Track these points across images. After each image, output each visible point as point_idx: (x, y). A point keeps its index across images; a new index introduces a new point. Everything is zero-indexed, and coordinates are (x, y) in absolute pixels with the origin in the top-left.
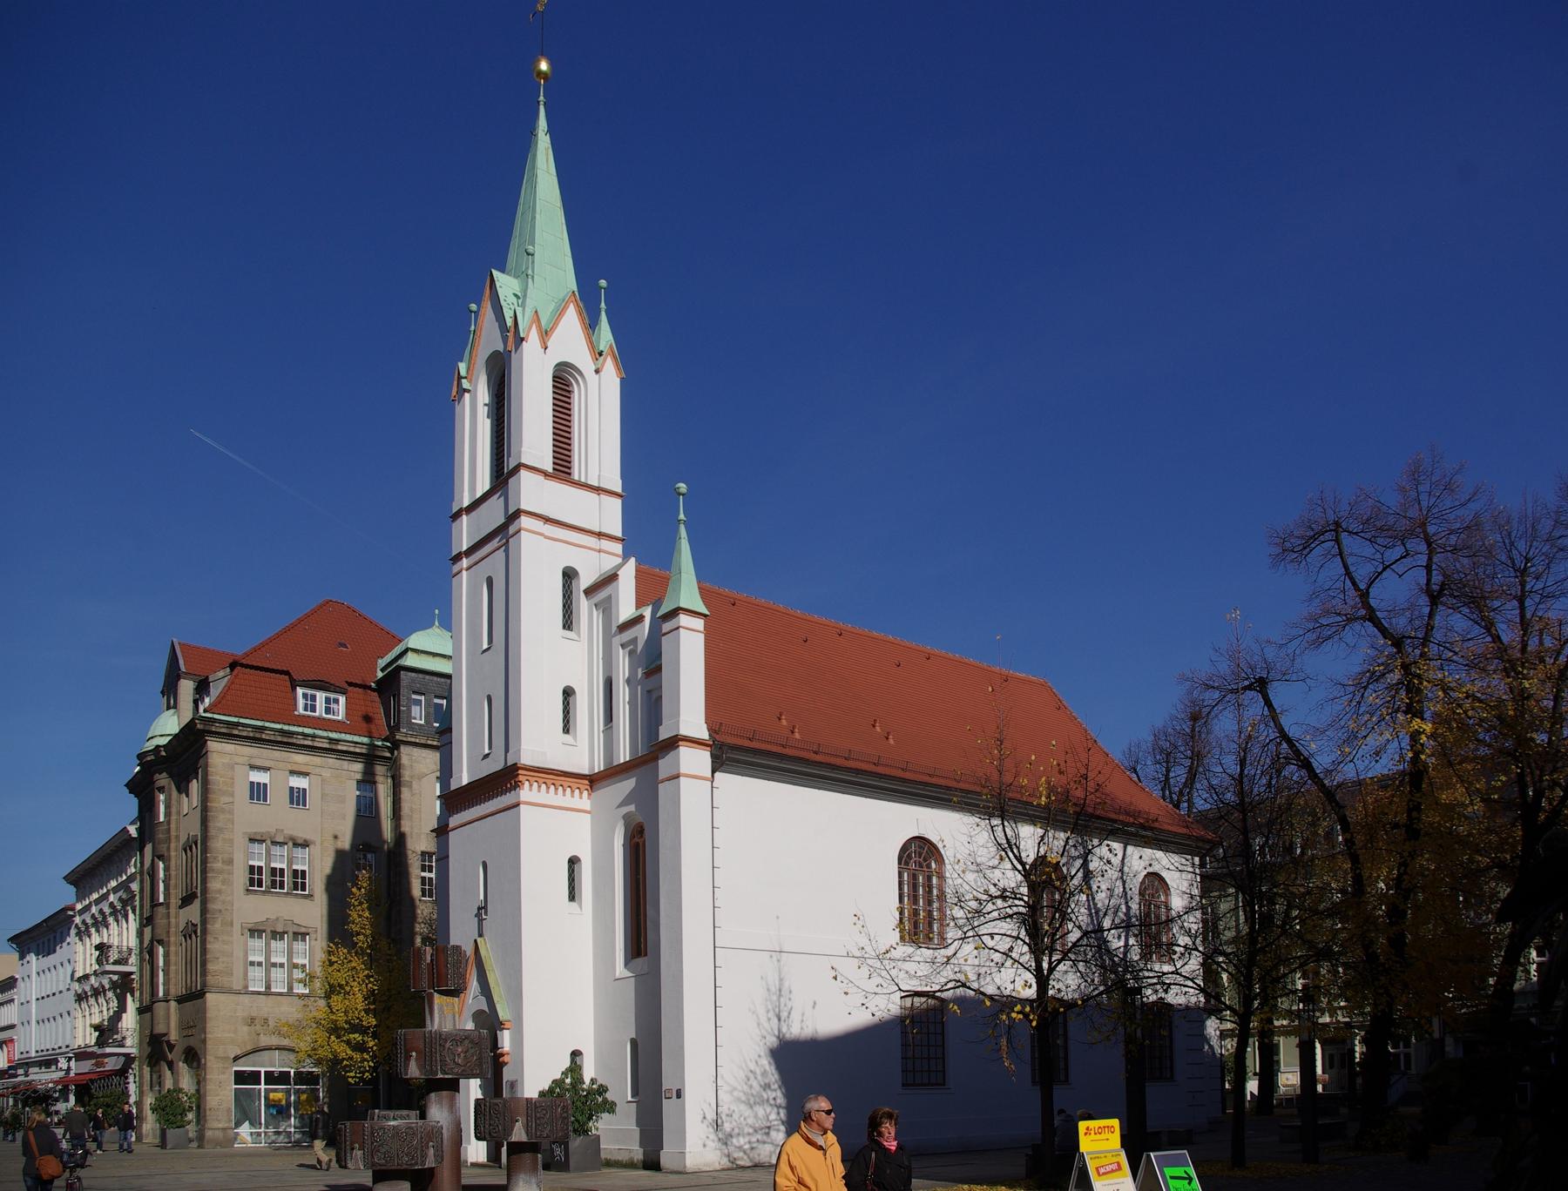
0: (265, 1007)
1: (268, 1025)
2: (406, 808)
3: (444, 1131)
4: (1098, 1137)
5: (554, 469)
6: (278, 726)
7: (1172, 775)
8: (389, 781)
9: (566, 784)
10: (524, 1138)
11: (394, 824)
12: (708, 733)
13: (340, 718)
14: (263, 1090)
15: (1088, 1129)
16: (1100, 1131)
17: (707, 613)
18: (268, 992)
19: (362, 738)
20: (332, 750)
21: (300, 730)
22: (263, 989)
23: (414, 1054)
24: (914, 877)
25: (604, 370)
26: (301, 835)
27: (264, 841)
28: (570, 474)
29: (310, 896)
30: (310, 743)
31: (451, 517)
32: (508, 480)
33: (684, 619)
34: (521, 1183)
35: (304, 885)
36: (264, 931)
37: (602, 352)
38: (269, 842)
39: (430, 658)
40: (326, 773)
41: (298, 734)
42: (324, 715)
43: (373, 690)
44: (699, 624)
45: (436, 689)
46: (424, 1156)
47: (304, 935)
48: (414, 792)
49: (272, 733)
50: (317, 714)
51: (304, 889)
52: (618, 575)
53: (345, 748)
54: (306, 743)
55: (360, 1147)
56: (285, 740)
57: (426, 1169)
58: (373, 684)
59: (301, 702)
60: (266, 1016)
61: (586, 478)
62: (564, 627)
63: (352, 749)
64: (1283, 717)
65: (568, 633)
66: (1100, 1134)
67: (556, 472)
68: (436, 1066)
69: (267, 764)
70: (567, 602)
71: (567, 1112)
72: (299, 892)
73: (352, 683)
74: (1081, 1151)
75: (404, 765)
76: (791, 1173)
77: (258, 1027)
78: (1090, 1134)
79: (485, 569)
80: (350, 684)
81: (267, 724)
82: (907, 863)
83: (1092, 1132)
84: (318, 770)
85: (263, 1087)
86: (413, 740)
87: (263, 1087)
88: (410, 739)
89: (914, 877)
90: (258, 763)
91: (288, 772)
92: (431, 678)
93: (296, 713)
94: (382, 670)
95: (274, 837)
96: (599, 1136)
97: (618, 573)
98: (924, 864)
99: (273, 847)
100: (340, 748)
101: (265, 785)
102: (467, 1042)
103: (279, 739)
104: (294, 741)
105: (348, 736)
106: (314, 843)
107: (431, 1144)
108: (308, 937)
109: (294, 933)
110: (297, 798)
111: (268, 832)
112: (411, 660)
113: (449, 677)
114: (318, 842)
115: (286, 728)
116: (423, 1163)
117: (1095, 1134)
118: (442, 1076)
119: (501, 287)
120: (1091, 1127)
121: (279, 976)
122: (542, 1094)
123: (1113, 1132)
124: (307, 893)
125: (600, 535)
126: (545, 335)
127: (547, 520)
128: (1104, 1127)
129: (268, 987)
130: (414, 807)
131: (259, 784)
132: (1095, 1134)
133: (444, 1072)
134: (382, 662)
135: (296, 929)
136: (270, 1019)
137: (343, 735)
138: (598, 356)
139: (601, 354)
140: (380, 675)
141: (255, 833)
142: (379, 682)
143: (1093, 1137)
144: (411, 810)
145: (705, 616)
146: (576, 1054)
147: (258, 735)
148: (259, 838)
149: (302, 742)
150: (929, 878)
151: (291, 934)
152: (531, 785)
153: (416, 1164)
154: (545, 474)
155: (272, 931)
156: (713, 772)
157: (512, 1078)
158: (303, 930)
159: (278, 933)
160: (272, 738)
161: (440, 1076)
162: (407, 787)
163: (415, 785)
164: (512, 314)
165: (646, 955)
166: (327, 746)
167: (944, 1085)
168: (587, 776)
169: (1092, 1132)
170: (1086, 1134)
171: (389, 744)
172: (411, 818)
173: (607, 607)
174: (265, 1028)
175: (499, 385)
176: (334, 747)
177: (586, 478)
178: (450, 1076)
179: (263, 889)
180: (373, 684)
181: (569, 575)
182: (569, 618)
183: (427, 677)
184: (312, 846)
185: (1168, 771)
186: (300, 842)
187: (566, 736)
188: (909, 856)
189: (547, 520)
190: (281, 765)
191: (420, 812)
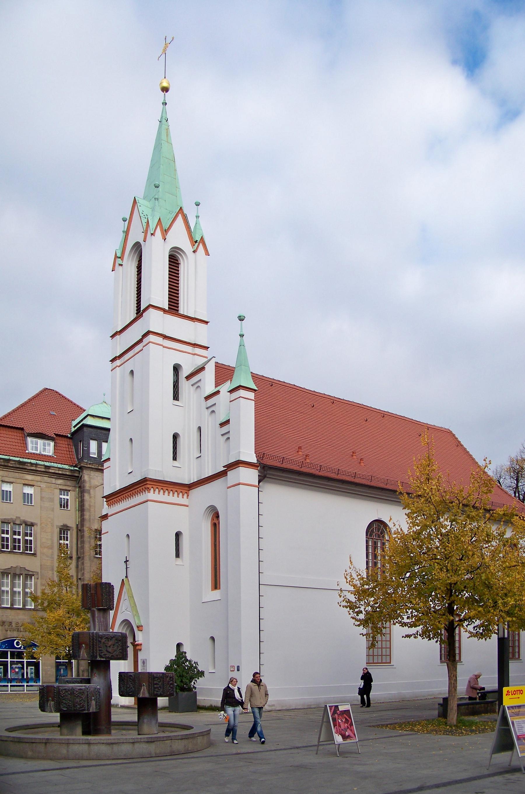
0: (10, 616)
1: (12, 626)
2: (87, 505)
3: (101, 691)
4: (514, 696)
5: (169, 308)
6: (17, 459)
7: (520, 484)
8: (77, 489)
9: (174, 490)
10: (147, 695)
11: (80, 515)
12: (256, 459)
13: (51, 454)
14: (9, 662)
15: (508, 692)
16: (515, 692)
17: (257, 389)
18: (12, 608)
19: (62, 465)
20: (47, 472)
21: (29, 461)
22: (9, 606)
23: (84, 645)
24: (375, 544)
25: (198, 251)
26: (30, 520)
27: (10, 523)
28: (178, 311)
29: (34, 555)
30: (34, 468)
31: (111, 337)
32: (142, 314)
33: (242, 393)
34: (145, 721)
35: (31, 548)
36: (10, 573)
37: (197, 241)
38: (12, 524)
39: (101, 420)
40: (43, 485)
41: (28, 463)
42: (42, 453)
43: (70, 438)
44: (251, 395)
45: (104, 437)
46: (89, 706)
47: (31, 576)
48: (91, 495)
49: (14, 463)
50: (38, 452)
51: (31, 550)
52: (205, 368)
53: (53, 471)
54: (32, 468)
55: (52, 699)
56: (21, 467)
57: (90, 713)
58: (69, 435)
59: (30, 446)
60: (11, 621)
61: (187, 312)
62: (174, 399)
63: (57, 472)
64: (524, 466)
65: (176, 402)
66: (515, 694)
67: (170, 310)
68: (96, 653)
69: (11, 480)
70: (175, 384)
71: (172, 680)
72: (29, 552)
73: (57, 434)
74: (504, 705)
75: (85, 480)
76: (346, 708)
77: (7, 627)
78: (509, 695)
79: (129, 366)
80: (57, 435)
81: (11, 458)
82: (371, 535)
83: (510, 694)
84: (39, 484)
85: (9, 660)
86: (91, 466)
87: (9, 660)
88: (89, 466)
89: (375, 544)
90: (6, 479)
91: (22, 485)
92: (101, 431)
93: (27, 451)
94: (74, 427)
95: (15, 521)
96: (196, 692)
97: (205, 367)
98: (381, 535)
99: (14, 526)
100: (50, 471)
101: (10, 492)
102: (114, 639)
103: (18, 466)
104: (26, 467)
105: (55, 464)
106: (36, 524)
107: (93, 698)
108: (33, 577)
109: (26, 574)
110: (27, 498)
111: (12, 519)
112: (90, 421)
113: (108, 430)
114: (39, 525)
115: (21, 460)
116: (88, 709)
117: (512, 694)
118: (100, 659)
119: (140, 206)
120: (510, 690)
121: (19, 599)
122: (167, 669)
123: (522, 694)
124: (33, 552)
125: (195, 345)
126: (165, 232)
127: (165, 337)
128: (517, 691)
129: (12, 604)
130: (91, 504)
131: (7, 491)
132: (512, 694)
133: (101, 657)
134: (74, 423)
135: (27, 573)
136: (13, 623)
137: (52, 463)
138: (194, 243)
139: (196, 242)
140: (73, 430)
141: (5, 519)
142: (73, 434)
143: (511, 696)
144: (90, 506)
145: (255, 390)
146: (179, 646)
147: (6, 464)
148: (7, 521)
149: (30, 468)
150: (383, 544)
151: (24, 575)
152: (154, 491)
153: (84, 710)
154: (164, 310)
155: (14, 574)
156: (259, 482)
157: (144, 658)
158: (31, 573)
159: (18, 574)
160: (14, 466)
161: (98, 658)
162: (87, 493)
163: (92, 492)
164: (146, 221)
165: (220, 588)
166: (44, 470)
167: (390, 663)
168: (188, 484)
169: (510, 694)
170: (507, 695)
171: (77, 469)
172: (89, 510)
173: (197, 386)
174: (10, 627)
175: (139, 261)
176: (47, 470)
177: (187, 312)
178: (104, 659)
179: (9, 550)
180: (69, 435)
181: (177, 369)
182: (175, 395)
183: (99, 431)
184: (35, 526)
185: (518, 482)
186: (29, 524)
187: (175, 461)
188: (372, 531)
189: (165, 337)
190: (19, 481)
191: (95, 507)
